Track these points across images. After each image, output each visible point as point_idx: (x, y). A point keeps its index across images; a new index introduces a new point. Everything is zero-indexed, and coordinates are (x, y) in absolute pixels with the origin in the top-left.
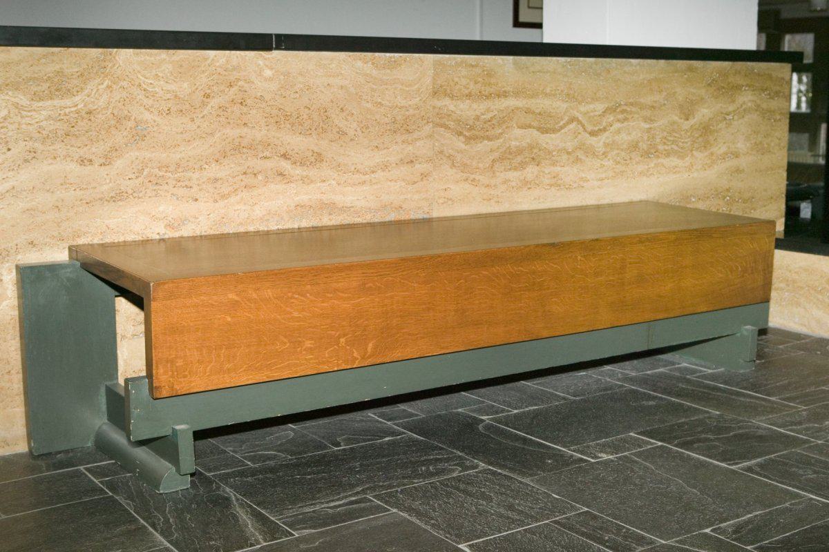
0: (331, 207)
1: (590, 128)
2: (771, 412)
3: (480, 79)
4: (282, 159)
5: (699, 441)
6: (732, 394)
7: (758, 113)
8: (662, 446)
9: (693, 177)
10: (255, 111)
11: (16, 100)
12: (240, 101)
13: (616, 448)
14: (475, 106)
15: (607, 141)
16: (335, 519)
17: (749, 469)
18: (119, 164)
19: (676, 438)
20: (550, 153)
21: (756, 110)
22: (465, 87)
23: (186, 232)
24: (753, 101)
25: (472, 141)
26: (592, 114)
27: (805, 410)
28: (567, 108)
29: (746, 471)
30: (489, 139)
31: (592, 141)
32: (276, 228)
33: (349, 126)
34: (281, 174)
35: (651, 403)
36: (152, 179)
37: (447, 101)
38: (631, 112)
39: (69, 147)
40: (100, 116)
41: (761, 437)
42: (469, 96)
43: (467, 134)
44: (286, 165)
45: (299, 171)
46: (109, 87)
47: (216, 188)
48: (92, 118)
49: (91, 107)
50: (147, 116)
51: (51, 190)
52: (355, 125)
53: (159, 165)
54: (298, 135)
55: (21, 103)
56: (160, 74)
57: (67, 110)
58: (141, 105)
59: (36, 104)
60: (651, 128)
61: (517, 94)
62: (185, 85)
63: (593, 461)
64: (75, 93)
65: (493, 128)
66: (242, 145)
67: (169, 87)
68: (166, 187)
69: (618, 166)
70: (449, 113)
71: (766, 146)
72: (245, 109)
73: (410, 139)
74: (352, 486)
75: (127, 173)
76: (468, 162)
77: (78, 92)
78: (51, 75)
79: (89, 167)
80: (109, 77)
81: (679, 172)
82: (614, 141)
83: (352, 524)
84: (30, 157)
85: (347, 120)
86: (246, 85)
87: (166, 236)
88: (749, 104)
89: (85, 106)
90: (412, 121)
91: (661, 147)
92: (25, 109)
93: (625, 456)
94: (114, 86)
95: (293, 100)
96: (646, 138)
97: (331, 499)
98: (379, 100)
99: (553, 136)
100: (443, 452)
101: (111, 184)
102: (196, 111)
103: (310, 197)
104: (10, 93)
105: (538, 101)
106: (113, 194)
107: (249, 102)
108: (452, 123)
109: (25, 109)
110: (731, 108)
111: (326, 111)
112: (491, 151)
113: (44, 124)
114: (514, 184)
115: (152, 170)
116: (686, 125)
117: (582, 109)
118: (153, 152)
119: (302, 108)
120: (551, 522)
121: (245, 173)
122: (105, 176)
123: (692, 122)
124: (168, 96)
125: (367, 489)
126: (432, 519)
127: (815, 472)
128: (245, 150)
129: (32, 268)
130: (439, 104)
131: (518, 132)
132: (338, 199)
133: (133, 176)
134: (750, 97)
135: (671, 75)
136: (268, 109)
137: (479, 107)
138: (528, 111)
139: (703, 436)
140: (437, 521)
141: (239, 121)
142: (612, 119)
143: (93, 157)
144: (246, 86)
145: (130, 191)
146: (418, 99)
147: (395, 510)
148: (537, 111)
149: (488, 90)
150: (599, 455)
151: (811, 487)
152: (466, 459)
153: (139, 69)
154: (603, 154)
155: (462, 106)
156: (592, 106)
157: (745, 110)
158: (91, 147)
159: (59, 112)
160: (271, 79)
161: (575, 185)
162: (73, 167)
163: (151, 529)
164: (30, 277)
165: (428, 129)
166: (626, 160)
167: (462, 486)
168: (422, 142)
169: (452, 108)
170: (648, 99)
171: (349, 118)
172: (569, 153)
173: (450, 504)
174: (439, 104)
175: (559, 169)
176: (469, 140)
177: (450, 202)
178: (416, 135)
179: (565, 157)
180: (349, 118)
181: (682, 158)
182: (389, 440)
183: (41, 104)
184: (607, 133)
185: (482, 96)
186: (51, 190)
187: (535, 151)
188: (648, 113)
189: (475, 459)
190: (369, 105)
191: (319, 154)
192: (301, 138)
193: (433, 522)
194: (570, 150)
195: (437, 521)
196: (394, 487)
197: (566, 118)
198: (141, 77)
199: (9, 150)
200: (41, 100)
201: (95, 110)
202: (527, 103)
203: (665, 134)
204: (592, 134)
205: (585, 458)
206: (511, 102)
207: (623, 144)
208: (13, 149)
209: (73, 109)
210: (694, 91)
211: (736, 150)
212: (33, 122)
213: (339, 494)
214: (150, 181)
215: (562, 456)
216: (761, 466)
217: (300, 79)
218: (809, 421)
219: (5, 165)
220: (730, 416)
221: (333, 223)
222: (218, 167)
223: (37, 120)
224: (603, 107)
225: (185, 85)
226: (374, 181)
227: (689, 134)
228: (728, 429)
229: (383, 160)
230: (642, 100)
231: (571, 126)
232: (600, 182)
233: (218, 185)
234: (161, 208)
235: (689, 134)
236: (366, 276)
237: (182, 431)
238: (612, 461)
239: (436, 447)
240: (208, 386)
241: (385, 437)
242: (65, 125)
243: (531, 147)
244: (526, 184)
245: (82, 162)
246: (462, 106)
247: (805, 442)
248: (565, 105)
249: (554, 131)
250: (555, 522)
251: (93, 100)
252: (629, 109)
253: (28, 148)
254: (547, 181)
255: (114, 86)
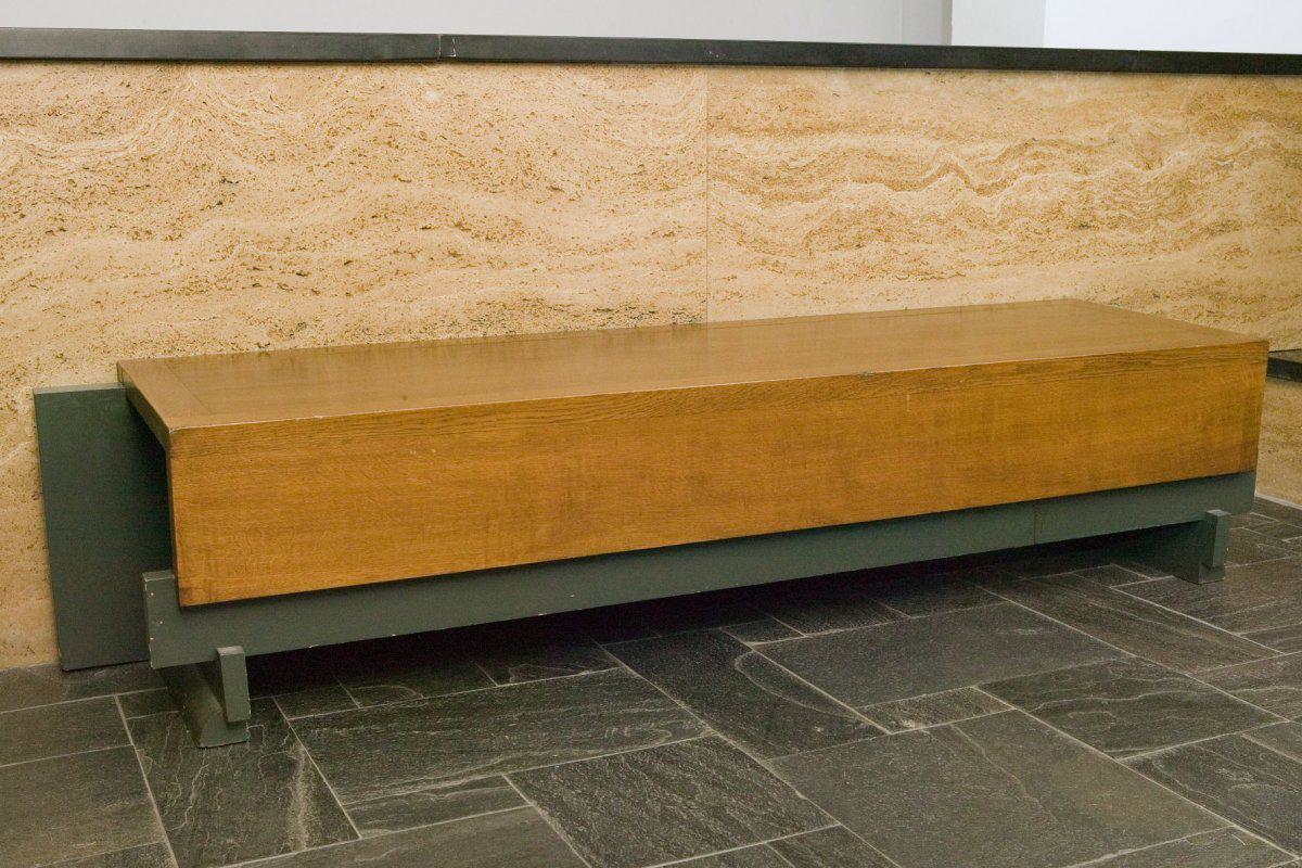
0: (537, 305)
1: (977, 181)
2: (1226, 659)
3: (789, 104)
4: (457, 230)
5: (1082, 706)
6: (1169, 622)
7: (1277, 157)
8: (1014, 712)
9: (1157, 262)
10: (412, 156)
11: (30, 141)
12: (387, 141)
13: (936, 712)
14: (779, 146)
15: (1008, 203)
16: (431, 813)
17: (1145, 766)
18: (194, 237)
19: (1042, 698)
20: (907, 221)
21: (1274, 153)
22: (762, 116)
23: (303, 341)
24: (1269, 137)
25: (775, 203)
26: (982, 159)
27: (1283, 658)
28: (938, 150)
29: (1139, 769)
30: (804, 198)
31: (983, 202)
32: (447, 336)
33: (568, 178)
34: (455, 255)
35: (1031, 632)
36: (247, 260)
37: (731, 140)
38: (1051, 156)
39: (115, 212)
40: (163, 164)
41: (1189, 705)
42: (770, 131)
43: (766, 191)
44: (462, 240)
45: (484, 249)
46: (177, 120)
47: (349, 275)
48: (151, 168)
49: (149, 151)
50: (237, 164)
51: (89, 278)
52: (576, 177)
53: (259, 239)
54: (481, 192)
55: (40, 145)
56: (259, 101)
57: (113, 156)
58: (228, 148)
59: (61, 147)
60: (1085, 182)
61: (852, 127)
62: (299, 116)
63: (889, 733)
64: (124, 131)
65: (810, 182)
66: (392, 209)
67: (272, 119)
68: (269, 273)
69: (1025, 243)
70: (734, 158)
71: (1289, 211)
72: (396, 153)
73: (669, 198)
74: (490, 753)
75: (207, 252)
76: (769, 236)
77: (127, 128)
78: (86, 102)
79: (148, 243)
80: (177, 105)
81: (1133, 253)
82: (1019, 202)
83: (454, 823)
84: (55, 228)
85: (563, 169)
86: (396, 115)
87: (270, 348)
88: (1262, 143)
89: (139, 149)
90: (672, 170)
91: (1101, 213)
92: (47, 154)
93: (947, 729)
94: (185, 118)
95: (473, 138)
96: (1075, 198)
97: (447, 775)
98: (619, 138)
99: (914, 194)
100: (660, 701)
101: (182, 269)
102: (316, 155)
103: (503, 289)
104: (22, 130)
105: (888, 138)
106: (186, 284)
107: (401, 140)
108: (741, 174)
109: (47, 154)
110: (1229, 149)
111: (528, 156)
112: (807, 217)
113: (76, 177)
114: (845, 270)
115: (246, 247)
116: (1147, 176)
117: (966, 150)
118: (247, 220)
119: (489, 151)
120: (771, 843)
121: (396, 252)
122: (173, 257)
123: (1157, 171)
124: (272, 133)
125: (508, 762)
126: (583, 823)
127: (1258, 779)
128: (395, 216)
129: (51, 397)
130: (720, 143)
131: (853, 188)
132: (550, 293)
133: (217, 256)
134: (1263, 132)
135: (1122, 95)
136: (433, 153)
137: (787, 149)
138: (870, 154)
139: (1091, 697)
140: (589, 828)
141: (386, 172)
142: (1017, 166)
143: (152, 228)
144: (398, 118)
145: (212, 280)
146: (683, 136)
147: (532, 804)
148: (888, 154)
149: (801, 122)
150: (905, 723)
151: (1240, 807)
152: (688, 718)
153: (224, 92)
154: (1000, 224)
155: (757, 147)
156: (981, 147)
157: (1252, 152)
158: (150, 212)
159: (99, 158)
160: (437, 106)
161: (950, 273)
162: (121, 243)
163: (156, 810)
164: (47, 406)
165: (698, 183)
166: (1040, 234)
167: (658, 767)
168: (690, 203)
169: (740, 149)
170: (1081, 135)
171: (566, 165)
172: (942, 223)
173: (624, 798)
174: (720, 143)
175: (924, 246)
176: (767, 200)
177: (736, 298)
178: (678, 193)
179: (933, 227)
180: (566, 165)
181: (1137, 229)
182: (587, 676)
183: (70, 146)
184: (1007, 190)
185: (794, 132)
186: (89, 278)
187: (881, 217)
188: (1079, 158)
189: (702, 716)
190: (601, 146)
191: (517, 223)
192: (489, 197)
193: (581, 829)
194: (943, 217)
195: (589, 828)
196: (552, 760)
197: (936, 167)
198: (228, 105)
199: (23, 216)
200: (70, 139)
201: (154, 155)
202: (869, 142)
203: (1110, 191)
204: (981, 191)
205: (879, 727)
206: (843, 140)
207: (1034, 208)
208: (28, 216)
209: (121, 154)
210: (1164, 122)
211: (1235, 218)
212: (59, 173)
213: (464, 766)
214: (244, 264)
215: (843, 721)
216: (1169, 761)
217: (485, 104)
218: (1284, 679)
219: (16, 239)
220: (1152, 662)
221: (540, 329)
222: (352, 242)
223: (65, 171)
224: (1001, 146)
225: (299, 116)
226: (608, 265)
227: (1152, 191)
228: (1142, 686)
229: (623, 231)
230: (1071, 138)
231: (947, 178)
232: (993, 269)
233: (350, 269)
234: (262, 305)
235: (1152, 191)
236: (532, 423)
237: (232, 657)
238: (921, 735)
239: (652, 693)
240: (532, 550)
241: (583, 670)
242: (109, 178)
243: (874, 211)
244: (867, 270)
245: (136, 235)
246: (757, 147)
247: (1263, 718)
248: (935, 145)
249: (914, 186)
250: (780, 845)
251: (151, 140)
252: (1046, 152)
253: (51, 213)
254: (901, 266)
255: (185, 118)
